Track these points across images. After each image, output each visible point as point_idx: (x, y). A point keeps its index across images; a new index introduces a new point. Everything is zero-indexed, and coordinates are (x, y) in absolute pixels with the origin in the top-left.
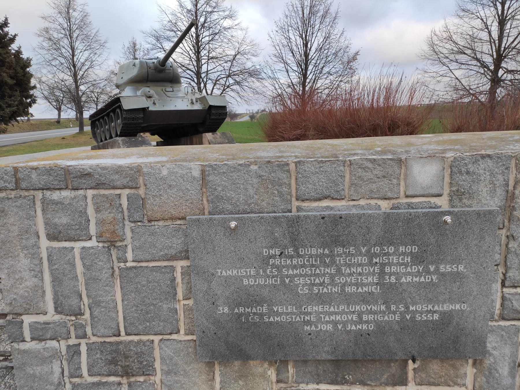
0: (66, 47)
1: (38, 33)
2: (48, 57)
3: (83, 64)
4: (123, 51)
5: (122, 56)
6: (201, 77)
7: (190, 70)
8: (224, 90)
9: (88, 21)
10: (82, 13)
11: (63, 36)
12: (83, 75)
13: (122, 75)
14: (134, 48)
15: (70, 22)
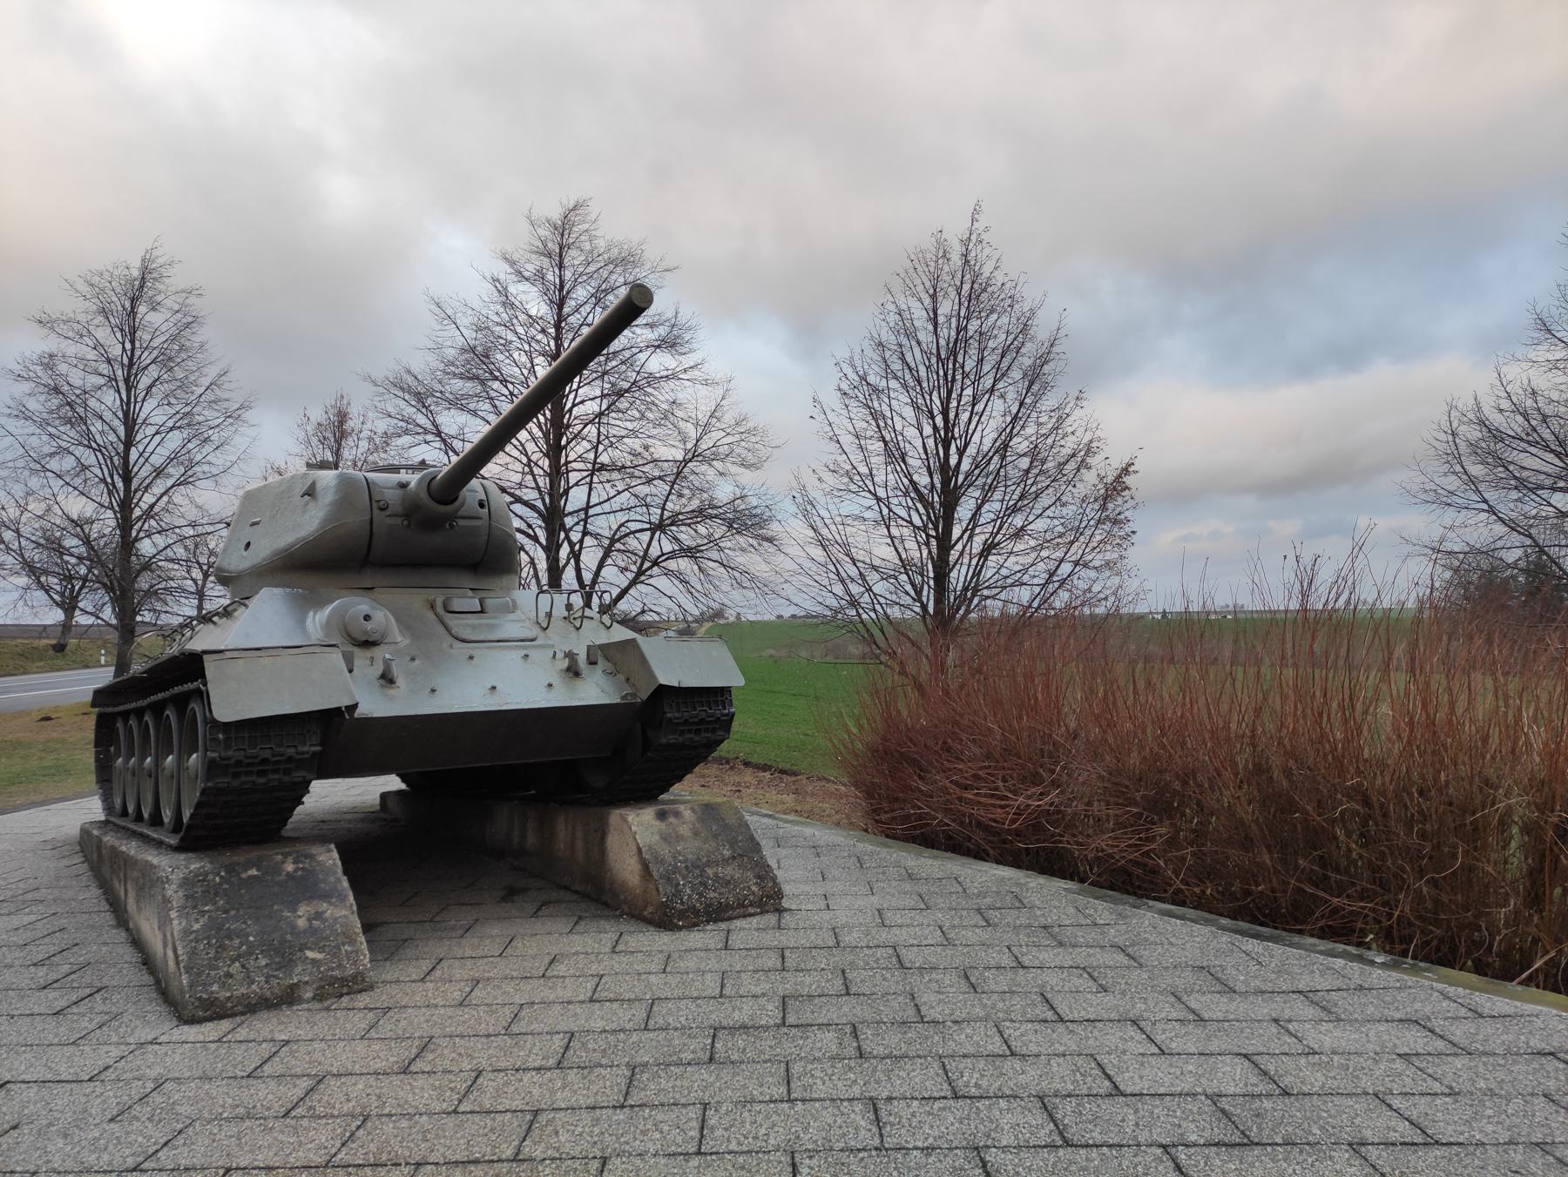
0: (108, 416)
1: (18, 369)
2: (40, 443)
3: (159, 472)
4: (302, 435)
5: (296, 449)
6: (563, 526)
7: (526, 504)
8: (640, 572)
9: (197, 339)
10: (179, 315)
11: (102, 381)
12: (152, 506)
13: (247, 534)
14: (338, 429)
15: (132, 342)
